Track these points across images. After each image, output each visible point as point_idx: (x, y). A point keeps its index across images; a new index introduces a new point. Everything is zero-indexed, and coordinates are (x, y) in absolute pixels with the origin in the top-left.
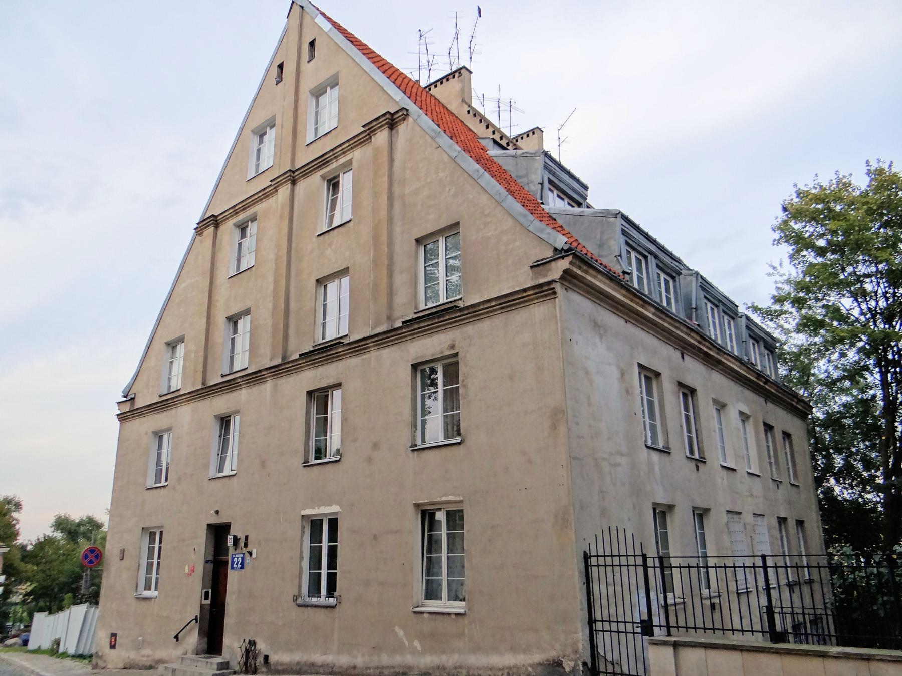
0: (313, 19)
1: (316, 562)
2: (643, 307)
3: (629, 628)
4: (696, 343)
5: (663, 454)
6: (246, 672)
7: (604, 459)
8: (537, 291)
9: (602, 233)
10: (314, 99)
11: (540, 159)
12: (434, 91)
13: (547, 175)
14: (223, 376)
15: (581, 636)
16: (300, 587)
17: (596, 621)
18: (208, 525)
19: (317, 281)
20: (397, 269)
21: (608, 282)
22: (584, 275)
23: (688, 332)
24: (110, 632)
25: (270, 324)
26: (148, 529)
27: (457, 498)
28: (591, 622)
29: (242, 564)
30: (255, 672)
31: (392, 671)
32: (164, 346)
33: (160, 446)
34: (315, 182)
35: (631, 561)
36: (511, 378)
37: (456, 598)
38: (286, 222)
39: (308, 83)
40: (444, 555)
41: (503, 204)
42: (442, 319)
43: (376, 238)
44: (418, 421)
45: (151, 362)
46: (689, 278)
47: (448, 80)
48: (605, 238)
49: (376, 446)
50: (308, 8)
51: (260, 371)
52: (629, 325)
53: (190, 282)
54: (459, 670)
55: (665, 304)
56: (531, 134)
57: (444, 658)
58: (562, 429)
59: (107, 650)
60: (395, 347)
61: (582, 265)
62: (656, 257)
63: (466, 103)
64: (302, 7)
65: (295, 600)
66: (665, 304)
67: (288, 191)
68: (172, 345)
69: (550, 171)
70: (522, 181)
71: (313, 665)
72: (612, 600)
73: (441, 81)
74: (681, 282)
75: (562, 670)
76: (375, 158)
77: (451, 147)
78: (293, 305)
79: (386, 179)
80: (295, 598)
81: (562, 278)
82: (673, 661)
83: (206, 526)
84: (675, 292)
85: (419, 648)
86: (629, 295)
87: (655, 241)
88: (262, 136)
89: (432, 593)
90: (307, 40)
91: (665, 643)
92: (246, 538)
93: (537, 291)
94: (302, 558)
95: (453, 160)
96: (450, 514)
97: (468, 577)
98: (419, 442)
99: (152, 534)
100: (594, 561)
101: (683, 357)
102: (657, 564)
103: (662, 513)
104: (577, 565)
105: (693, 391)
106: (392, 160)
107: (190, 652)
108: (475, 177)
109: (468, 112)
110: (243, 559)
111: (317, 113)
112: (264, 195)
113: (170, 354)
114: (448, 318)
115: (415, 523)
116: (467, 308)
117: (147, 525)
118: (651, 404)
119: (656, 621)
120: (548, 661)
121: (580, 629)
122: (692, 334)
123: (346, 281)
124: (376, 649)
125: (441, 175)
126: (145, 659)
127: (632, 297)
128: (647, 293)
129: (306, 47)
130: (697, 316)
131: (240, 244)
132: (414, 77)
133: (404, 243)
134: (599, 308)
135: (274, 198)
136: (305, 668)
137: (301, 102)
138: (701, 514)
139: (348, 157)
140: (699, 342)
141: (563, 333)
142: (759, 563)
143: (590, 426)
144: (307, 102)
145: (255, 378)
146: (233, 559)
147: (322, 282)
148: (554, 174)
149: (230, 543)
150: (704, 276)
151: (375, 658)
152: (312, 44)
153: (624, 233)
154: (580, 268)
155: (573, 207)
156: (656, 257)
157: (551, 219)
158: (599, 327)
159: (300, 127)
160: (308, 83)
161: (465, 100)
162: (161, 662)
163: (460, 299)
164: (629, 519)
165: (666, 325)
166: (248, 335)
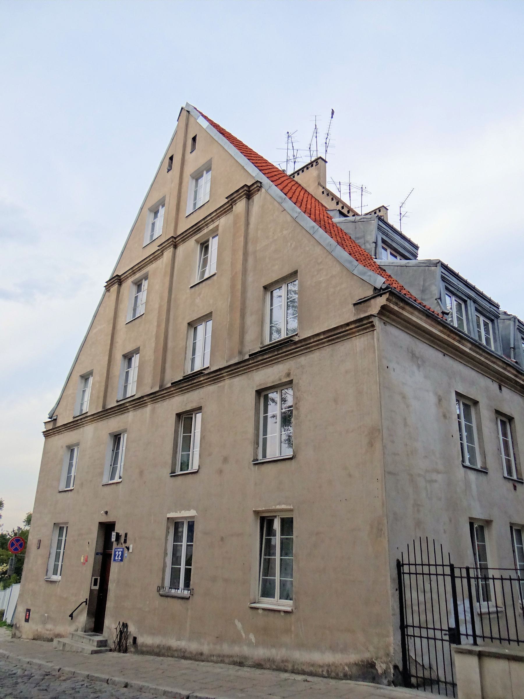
0: (196, 119)
1: (176, 559)
2: (459, 342)
3: (438, 634)
4: (513, 377)
5: (480, 474)
6: (119, 651)
7: (419, 475)
8: (357, 325)
9: (424, 280)
10: (194, 181)
11: (375, 223)
12: (297, 178)
13: (380, 236)
14: (118, 402)
15: (393, 640)
16: (163, 579)
17: (407, 626)
18: (100, 523)
19: (189, 324)
20: (248, 311)
21: (424, 318)
22: (400, 311)
23: (505, 366)
24: (26, 608)
25: (153, 358)
26: (58, 524)
27: (288, 507)
28: (403, 627)
29: (122, 556)
30: (125, 651)
31: (231, 659)
32: (79, 378)
33: (71, 458)
34: (191, 245)
35: (440, 570)
36: (336, 401)
37: (288, 597)
38: (168, 278)
39: (190, 169)
40: (278, 557)
41: (333, 253)
43: (233, 287)
44: (260, 439)
45: (69, 391)
46: (507, 322)
47: (308, 168)
48: (427, 284)
49: (225, 460)
50: (193, 113)
51: (142, 397)
52: (447, 358)
54: (286, 664)
55: (484, 342)
57: (274, 651)
58: (378, 445)
60: (244, 376)
62: (475, 301)
63: (321, 186)
64: (188, 112)
65: (158, 591)
66: (484, 342)
68: (85, 378)
69: (384, 233)
70: (360, 242)
71: (169, 648)
72: (429, 606)
73: (302, 170)
74: (500, 325)
75: (374, 671)
76: (235, 223)
77: (293, 209)
78: (170, 344)
79: (242, 239)
80: (159, 589)
82: (478, 670)
84: (494, 333)
85: (253, 640)
86: (445, 331)
87: (474, 288)
88: (156, 213)
89: (267, 591)
90: (191, 136)
91: (470, 652)
92: (126, 535)
93: (357, 325)
94: (166, 554)
95: (294, 219)
96: (283, 520)
98: (260, 457)
99: (61, 528)
100: (406, 569)
101: (500, 389)
102: (464, 574)
103: (478, 529)
104: (388, 574)
105: (511, 419)
106: (247, 224)
107: (80, 629)
108: (311, 232)
109: (323, 193)
110: (123, 552)
111: (196, 192)
112: (154, 257)
113: (83, 384)
114: (285, 350)
115: (254, 528)
116: (300, 341)
118: (469, 429)
119: (462, 630)
120: (362, 661)
121: (392, 633)
122: (508, 368)
123: (210, 324)
124: (219, 639)
125: (285, 232)
126: (48, 632)
127: (448, 333)
128: (466, 332)
129: (190, 142)
130: (515, 354)
131: (136, 297)
132: (282, 167)
133: (254, 290)
134: (418, 342)
135: (161, 260)
136: (163, 651)
137: (184, 184)
139: (211, 227)
140: (516, 376)
141: (380, 360)
143: (406, 445)
144: (189, 183)
145: (138, 402)
146: (115, 552)
147: (192, 325)
148: (387, 235)
149: (113, 539)
150: (446, 263)
151: (218, 647)
152: (194, 139)
153: (443, 279)
154: (397, 304)
156: (475, 301)
157: (381, 270)
158: (418, 358)
159: (182, 203)
160: (190, 169)
161: (321, 184)
162: (59, 636)
163: (297, 335)
164: (445, 532)
166: (137, 369)
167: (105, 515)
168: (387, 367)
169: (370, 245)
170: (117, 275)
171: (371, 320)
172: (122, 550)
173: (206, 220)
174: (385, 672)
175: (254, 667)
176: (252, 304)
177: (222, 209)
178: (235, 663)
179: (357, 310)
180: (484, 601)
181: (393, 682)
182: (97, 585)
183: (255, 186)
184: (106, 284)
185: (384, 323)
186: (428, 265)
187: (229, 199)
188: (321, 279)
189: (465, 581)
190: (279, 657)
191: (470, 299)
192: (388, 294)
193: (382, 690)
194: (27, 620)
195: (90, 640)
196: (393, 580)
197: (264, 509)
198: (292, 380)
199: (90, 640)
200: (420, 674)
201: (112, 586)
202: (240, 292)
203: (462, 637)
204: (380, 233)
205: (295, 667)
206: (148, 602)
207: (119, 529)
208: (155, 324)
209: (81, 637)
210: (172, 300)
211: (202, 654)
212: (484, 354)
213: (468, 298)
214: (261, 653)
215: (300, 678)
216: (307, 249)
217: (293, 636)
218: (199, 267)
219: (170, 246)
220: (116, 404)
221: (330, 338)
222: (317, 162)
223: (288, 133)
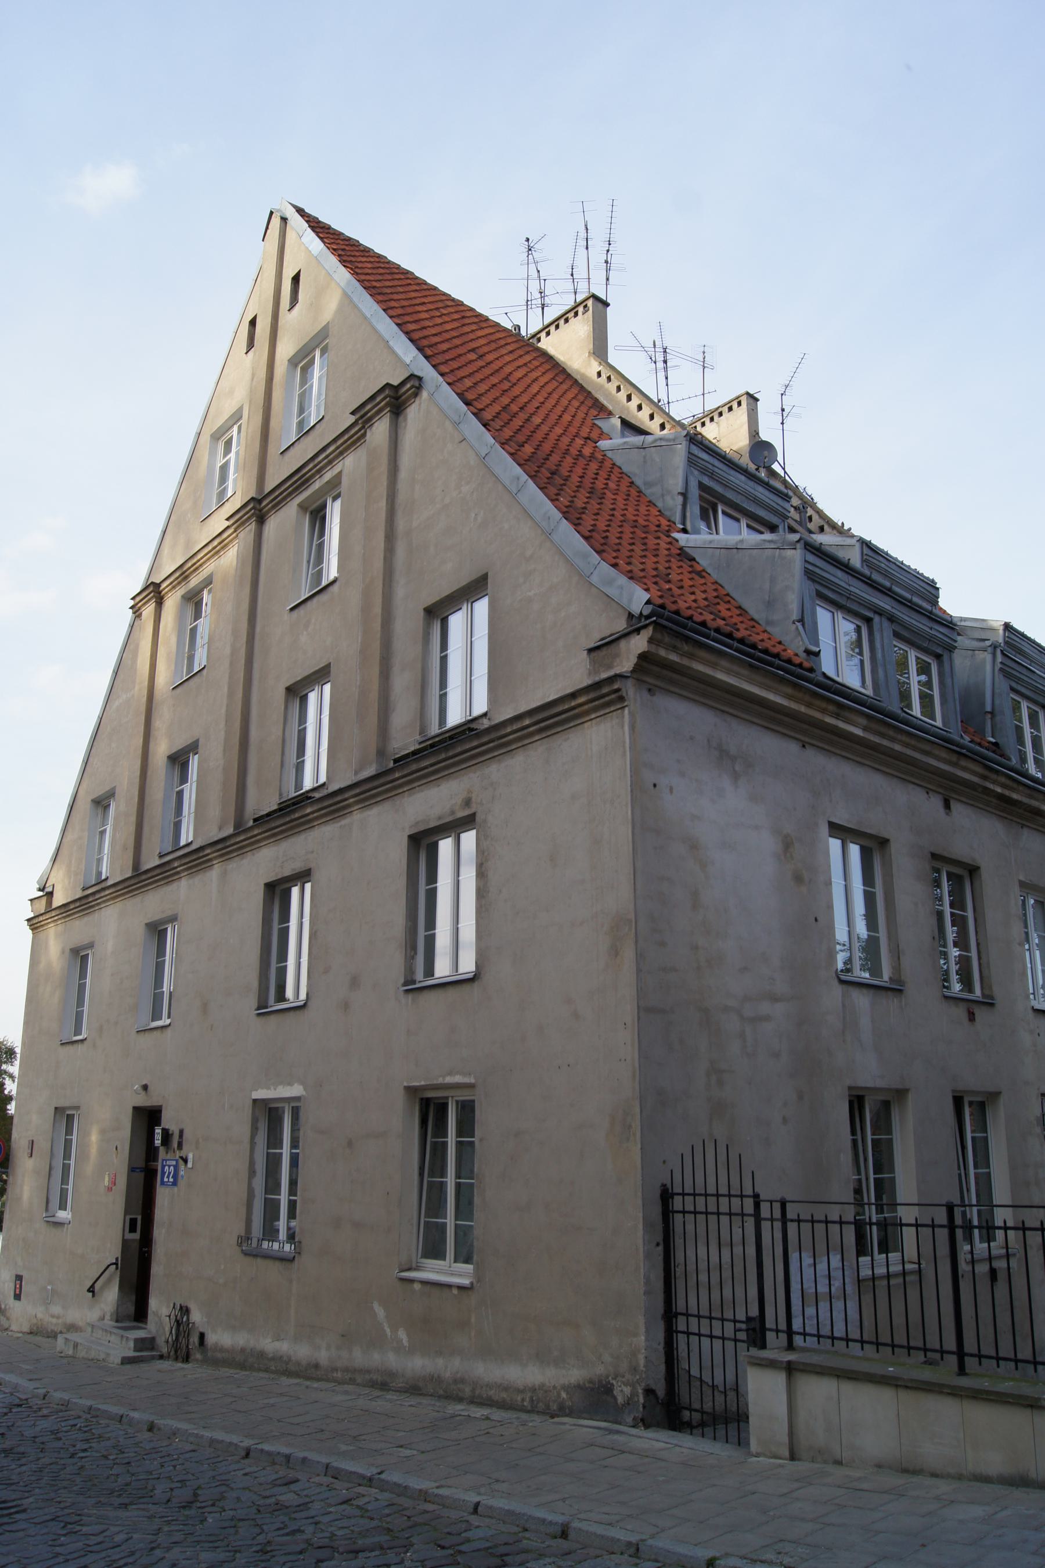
2: (837, 716)
6: (176, 1359)
8: (592, 695)
17: (677, 1314)
18: (135, 1109)
21: (745, 672)
22: (685, 662)
23: (954, 758)
24: (14, 1273)
30: (187, 1359)
31: (367, 1377)
37: (467, 1260)
42: (451, 753)
43: (366, 609)
46: (981, 655)
47: (567, 321)
49: (355, 982)
52: (810, 752)
53: (124, 697)
54: (461, 1386)
55: (916, 710)
56: (735, 405)
57: (440, 1362)
59: (11, 1301)
60: (387, 806)
61: (678, 644)
62: (892, 619)
65: (240, 1245)
67: (251, 537)
68: (101, 804)
69: (704, 471)
71: (261, 1355)
73: (555, 323)
78: (254, 734)
79: (383, 504)
81: (637, 669)
83: (131, 1110)
85: (405, 1342)
92: (181, 1132)
93: (592, 695)
97: (479, 1222)
98: (419, 975)
100: (677, 1203)
101: (947, 806)
102: (777, 1214)
107: (108, 1317)
110: (176, 1167)
114: (459, 749)
117: (61, 1103)
119: (770, 1323)
120: (591, 1381)
121: (642, 1329)
122: (963, 763)
126: (54, 1320)
127: (807, 698)
138: (971, 1107)
139: (328, 476)
140: (984, 778)
142: (941, 1217)
145: (196, 859)
149: (158, 1142)
152: (296, 279)
154: (675, 649)
155: (762, 533)
156: (892, 619)
162: (72, 1328)
164: (785, 1120)
165: (897, 747)
167: (143, 1093)
168: (655, 785)
169: (674, 499)
170: (152, 583)
171: (616, 687)
172: (174, 1163)
173: (316, 461)
174: (629, 1402)
175: (405, 1392)
176: (405, 647)
177: (346, 437)
178: (373, 1384)
179: (593, 662)
180: (880, 1253)
181: (642, 1420)
182: (135, 1231)
183: (408, 386)
184: (132, 603)
185: (650, 690)
186: (779, 545)
187: (358, 416)
188: (531, 594)
189: (778, 1225)
190: (448, 1374)
191: (880, 615)
192: (651, 628)
193: (616, 1437)
194: (17, 1297)
195: (122, 1336)
196: (648, 1224)
197: (423, 1083)
198: (474, 815)
199: (122, 1336)
200: (708, 1406)
201: (159, 1233)
202: (379, 620)
203: (768, 1333)
204: (696, 472)
205: (477, 1392)
206: (222, 1267)
207: (169, 1121)
208: (226, 689)
209: (106, 1331)
210: (257, 637)
211: (317, 1366)
212: (899, 737)
213: (875, 612)
214: (418, 1365)
215: (479, 1412)
216: (506, 526)
217: (473, 1334)
218: (309, 562)
219: (249, 518)
220: (157, 862)
221: (542, 725)
222: (586, 306)
223: (528, 240)
